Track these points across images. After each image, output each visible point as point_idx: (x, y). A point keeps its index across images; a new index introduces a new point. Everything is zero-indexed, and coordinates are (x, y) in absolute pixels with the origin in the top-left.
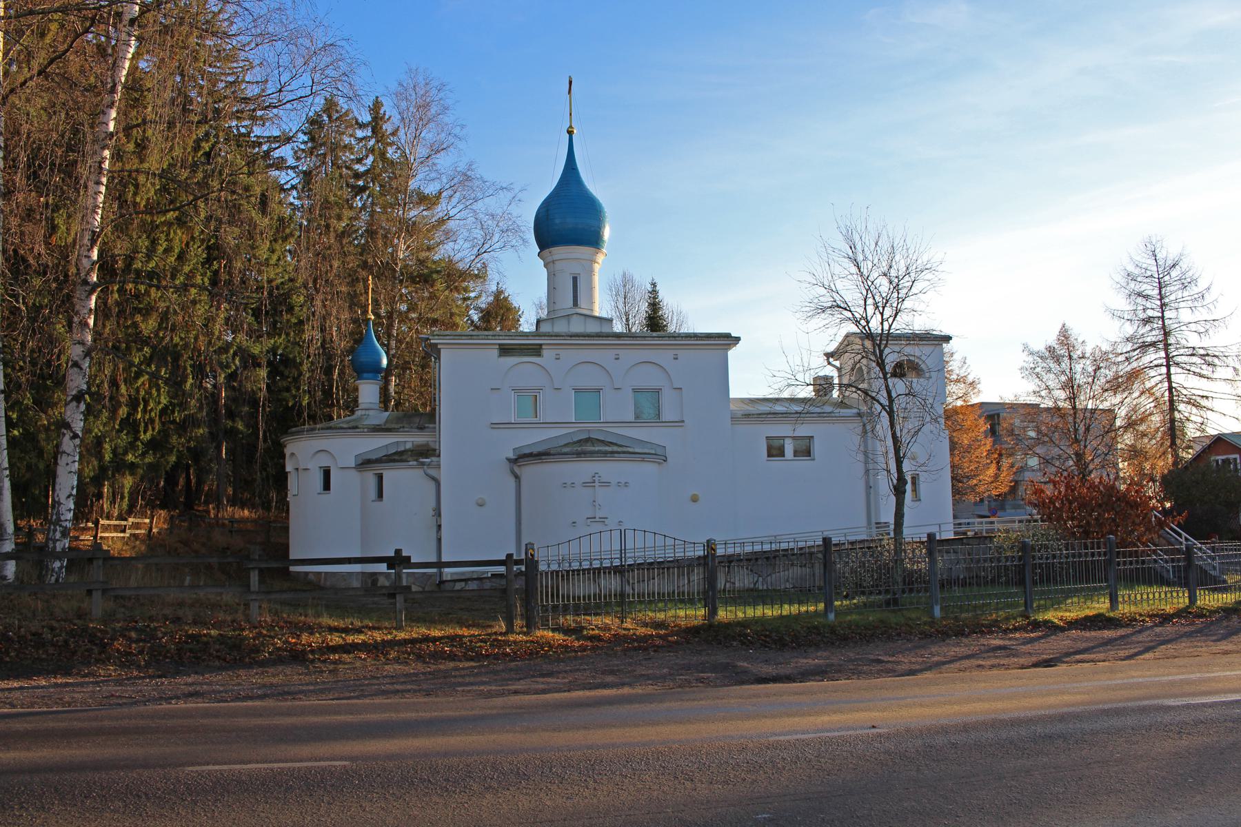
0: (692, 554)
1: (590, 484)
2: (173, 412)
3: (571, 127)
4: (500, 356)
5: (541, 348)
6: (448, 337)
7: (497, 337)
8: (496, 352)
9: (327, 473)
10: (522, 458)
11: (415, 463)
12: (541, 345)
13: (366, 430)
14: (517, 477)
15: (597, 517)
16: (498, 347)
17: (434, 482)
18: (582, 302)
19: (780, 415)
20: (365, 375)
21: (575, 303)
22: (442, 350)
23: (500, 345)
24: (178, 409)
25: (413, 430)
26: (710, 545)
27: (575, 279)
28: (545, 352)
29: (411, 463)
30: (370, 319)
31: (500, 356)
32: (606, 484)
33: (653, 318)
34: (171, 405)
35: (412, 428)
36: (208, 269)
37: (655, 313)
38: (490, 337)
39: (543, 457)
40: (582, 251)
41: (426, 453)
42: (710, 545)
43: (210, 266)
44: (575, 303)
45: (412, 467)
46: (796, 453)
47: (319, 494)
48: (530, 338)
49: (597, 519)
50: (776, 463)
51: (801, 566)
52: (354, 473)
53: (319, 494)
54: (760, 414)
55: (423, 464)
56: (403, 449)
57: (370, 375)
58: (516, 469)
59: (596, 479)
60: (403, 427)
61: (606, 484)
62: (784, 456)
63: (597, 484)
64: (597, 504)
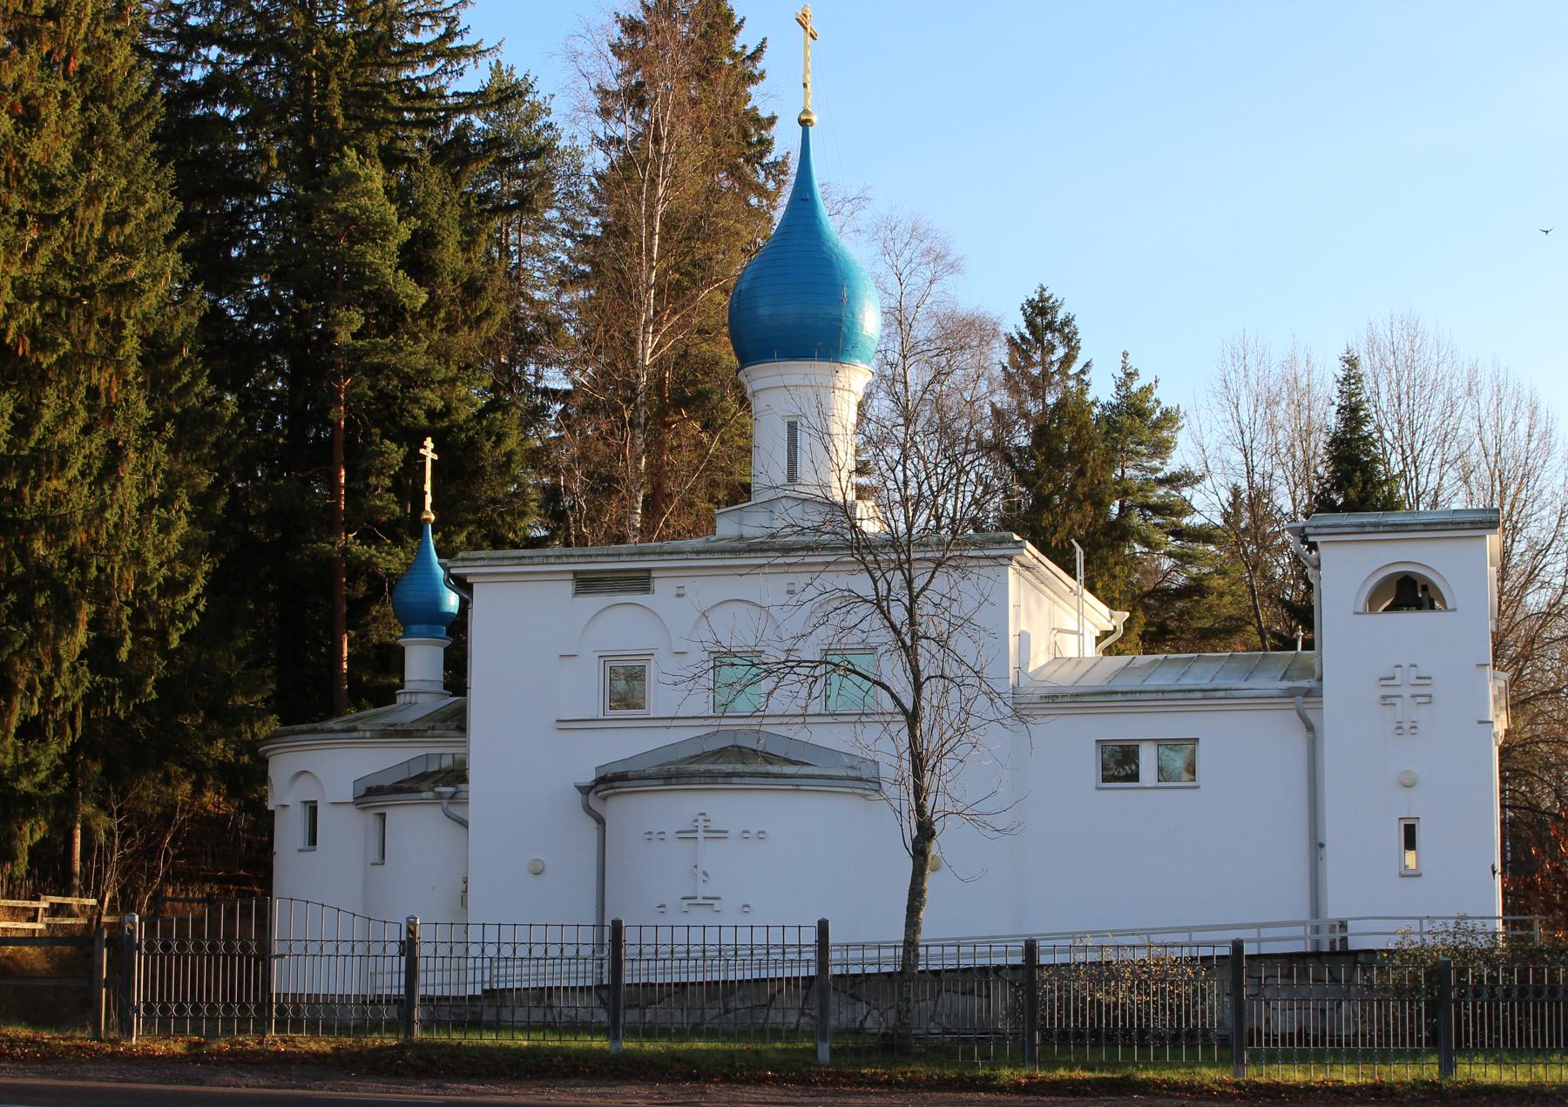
0: (971, 961)
1: (687, 835)
2: (111, 701)
3: (806, 112)
4: (577, 593)
5: (649, 577)
6: (479, 563)
7: (565, 560)
8: (569, 587)
9: (312, 808)
10: (610, 782)
11: (430, 794)
12: (649, 570)
13: (368, 734)
14: (601, 821)
15: (699, 897)
16: (571, 577)
17: (594, 825)
18: (805, 472)
19: (1119, 697)
20: (414, 628)
21: (792, 475)
22: (475, 586)
23: (575, 573)
24: (119, 695)
25: (451, 733)
26: (1237, 946)
27: (792, 428)
28: (658, 585)
29: (424, 795)
30: (427, 520)
31: (577, 593)
32: (720, 835)
33: (1349, 442)
34: (107, 687)
35: (448, 729)
36: (156, 437)
37: (1354, 430)
38: (553, 560)
39: (616, 784)
40: (814, 370)
41: (457, 775)
42: (1237, 946)
43: (160, 432)
44: (792, 475)
45: (424, 802)
46: (1163, 773)
47: (300, 851)
48: (623, 558)
49: (700, 901)
50: (1121, 795)
51: (963, 993)
52: (353, 810)
53: (300, 851)
54: (1077, 695)
55: (440, 796)
56: (436, 768)
57: (424, 628)
58: (594, 803)
59: (701, 825)
60: (433, 728)
61: (720, 835)
62: (1137, 780)
63: (701, 835)
64: (699, 871)
